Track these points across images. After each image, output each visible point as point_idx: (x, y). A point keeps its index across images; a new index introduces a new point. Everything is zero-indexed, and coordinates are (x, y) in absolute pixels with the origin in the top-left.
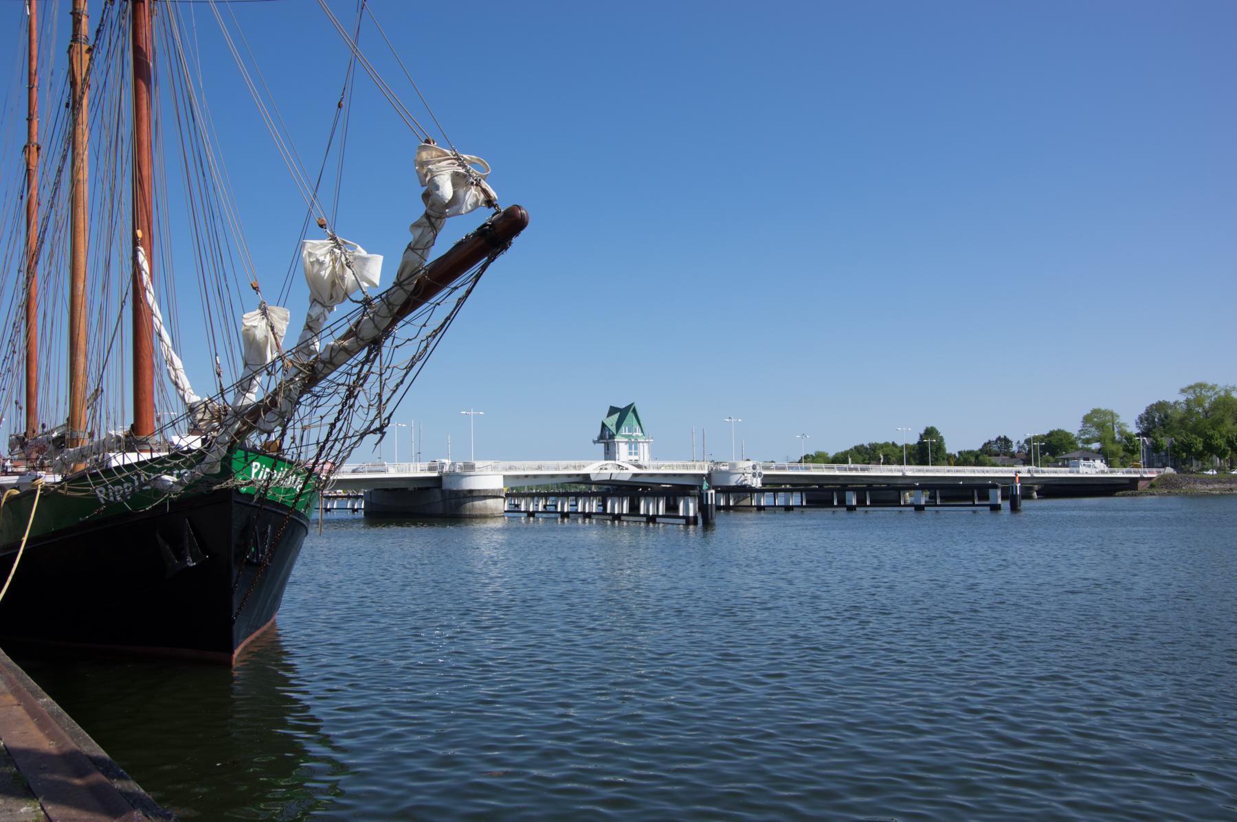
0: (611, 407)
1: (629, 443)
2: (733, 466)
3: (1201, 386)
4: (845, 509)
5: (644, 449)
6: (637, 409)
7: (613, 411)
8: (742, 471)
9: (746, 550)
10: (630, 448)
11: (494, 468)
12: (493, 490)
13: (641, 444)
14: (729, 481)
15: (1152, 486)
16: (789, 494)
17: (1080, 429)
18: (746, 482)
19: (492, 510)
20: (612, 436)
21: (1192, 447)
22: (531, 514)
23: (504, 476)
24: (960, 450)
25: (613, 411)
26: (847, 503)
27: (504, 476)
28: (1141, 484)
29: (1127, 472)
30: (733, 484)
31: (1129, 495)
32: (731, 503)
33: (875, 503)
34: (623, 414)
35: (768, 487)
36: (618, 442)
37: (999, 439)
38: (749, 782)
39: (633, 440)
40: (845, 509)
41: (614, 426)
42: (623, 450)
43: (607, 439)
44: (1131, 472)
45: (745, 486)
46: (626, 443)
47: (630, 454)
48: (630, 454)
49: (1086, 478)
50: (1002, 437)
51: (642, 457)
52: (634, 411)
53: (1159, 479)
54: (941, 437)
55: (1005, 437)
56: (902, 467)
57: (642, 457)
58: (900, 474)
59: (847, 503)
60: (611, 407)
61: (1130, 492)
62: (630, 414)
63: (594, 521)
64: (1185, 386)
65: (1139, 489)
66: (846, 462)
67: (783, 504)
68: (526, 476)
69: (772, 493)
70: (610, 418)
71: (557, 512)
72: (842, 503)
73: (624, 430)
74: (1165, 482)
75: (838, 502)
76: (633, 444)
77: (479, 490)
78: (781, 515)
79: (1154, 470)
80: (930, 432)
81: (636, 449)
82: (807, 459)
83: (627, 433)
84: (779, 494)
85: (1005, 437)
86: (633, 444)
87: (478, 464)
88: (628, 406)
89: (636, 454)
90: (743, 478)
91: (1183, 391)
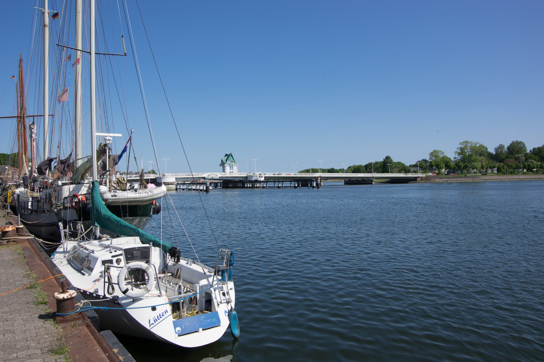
0: (226, 154)
1: (230, 167)
2: (254, 174)
3: (467, 142)
4: (312, 187)
5: (235, 169)
6: (233, 155)
7: (226, 155)
8: (256, 176)
9: (220, 199)
10: (230, 168)
11: (172, 176)
12: (171, 182)
13: (234, 166)
14: (252, 178)
15: (422, 180)
16: (279, 183)
17: (429, 157)
18: (258, 179)
19: (170, 188)
20: (224, 164)
21: (439, 166)
22: (183, 189)
23: (176, 178)
24: (410, 164)
25: (226, 155)
26: (313, 186)
27: (176, 178)
28: (418, 179)
29: (413, 175)
30: (254, 180)
31: (412, 183)
32: (251, 186)
33: (302, 186)
34: (228, 156)
35: (266, 180)
36: (226, 166)
37: (423, 160)
38: (241, 263)
39: (231, 165)
40: (312, 187)
41: (225, 161)
42: (228, 169)
43: (223, 164)
44: (414, 175)
45: (257, 180)
46: (229, 166)
47: (230, 170)
48: (230, 170)
49: (290, 177)
50: (424, 159)
51: (234, 171)
52: (232, 155)
53: (425, 177)
54: (392, 160)
55: (425, 159)
56: (372, 174)
57: (234, 171)
58: (371, 176)
59: (313, 186)
60: (226, 154)
61: (413, 182)
62: (230, 156)
63: (185, 191)
64: (461, 142)
65: (418, 181)
66: (310, 172)
67: (277, 186)
68: (184, 178)
69: (290, 182)
70: (225, 157)
71: (181, 189)
72: (311, 185)
73: (228, 162)
74: (427, 179)
75: (310, 185)
76: (231, 167)
77: (166, 182)
78: (277, 190)
79: (424, 174)
80: (388, 158)
81: (232, 168)
82: (302, 172)
83: (229, 163)
84: (292, 182)
85: (425, 159)
86: (231, 167)
87: (166, 174)
88: (120, 159)
89: (232, 170)
90: (257, 178)
91: (460, 144)
